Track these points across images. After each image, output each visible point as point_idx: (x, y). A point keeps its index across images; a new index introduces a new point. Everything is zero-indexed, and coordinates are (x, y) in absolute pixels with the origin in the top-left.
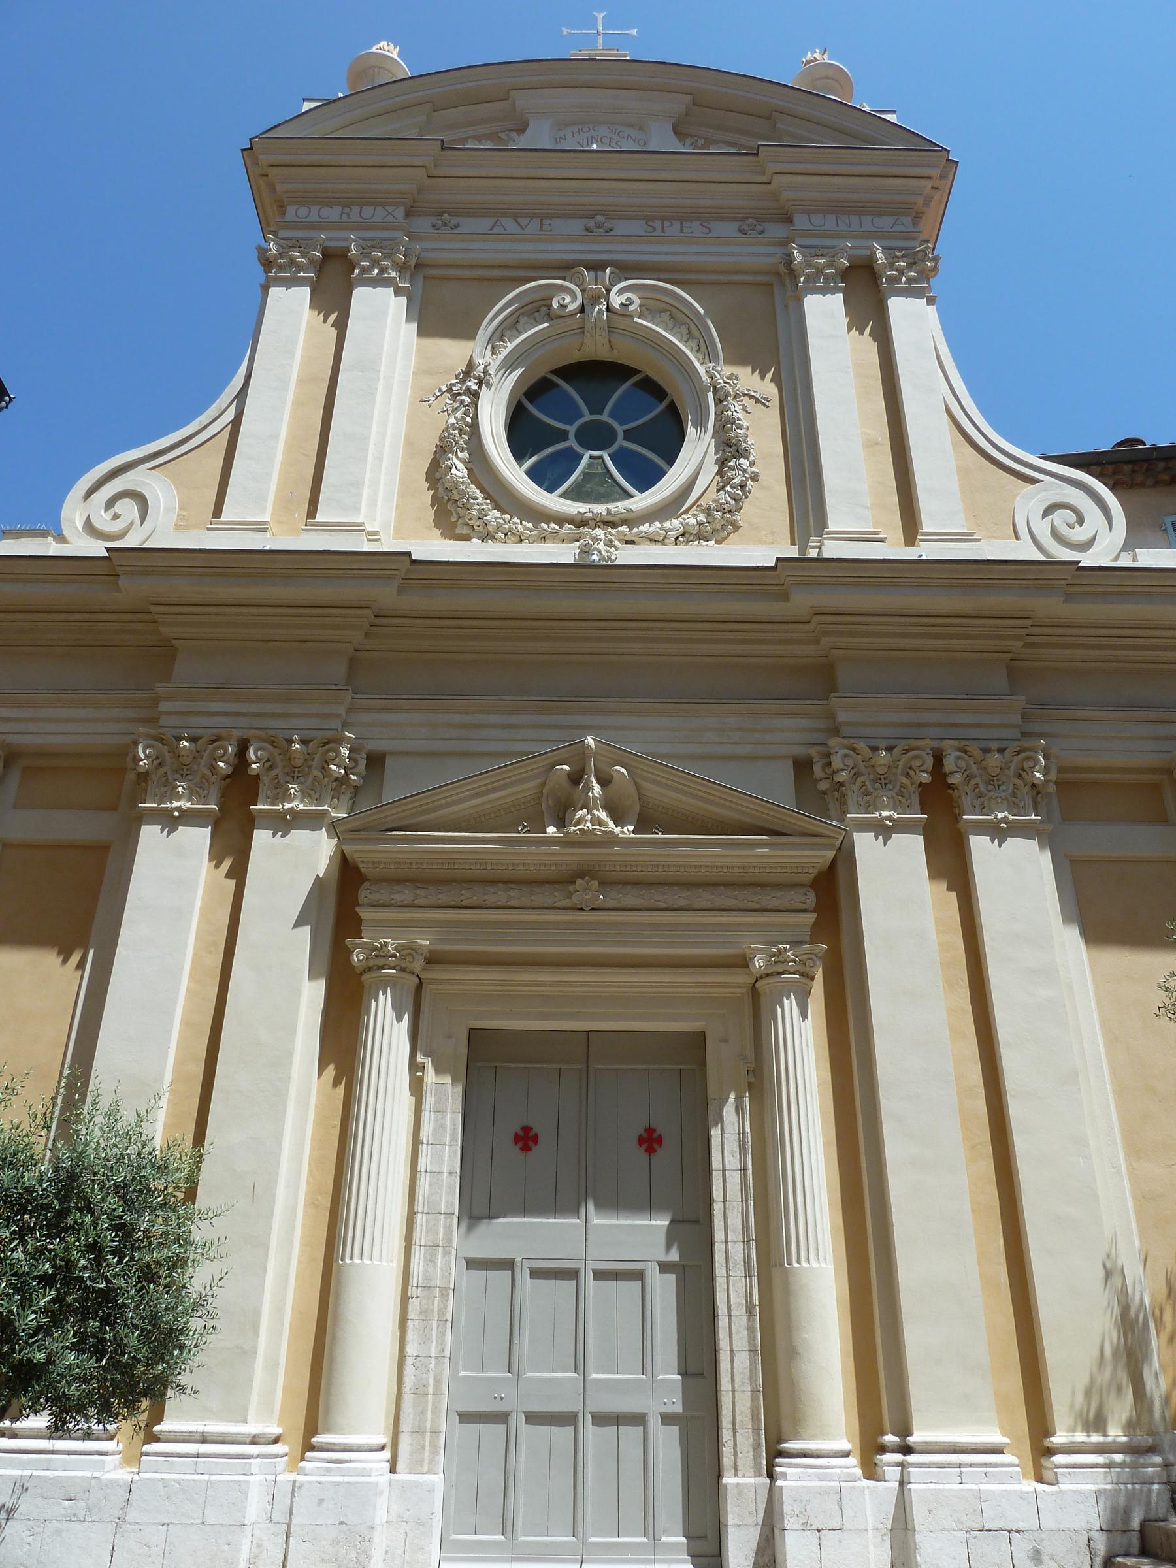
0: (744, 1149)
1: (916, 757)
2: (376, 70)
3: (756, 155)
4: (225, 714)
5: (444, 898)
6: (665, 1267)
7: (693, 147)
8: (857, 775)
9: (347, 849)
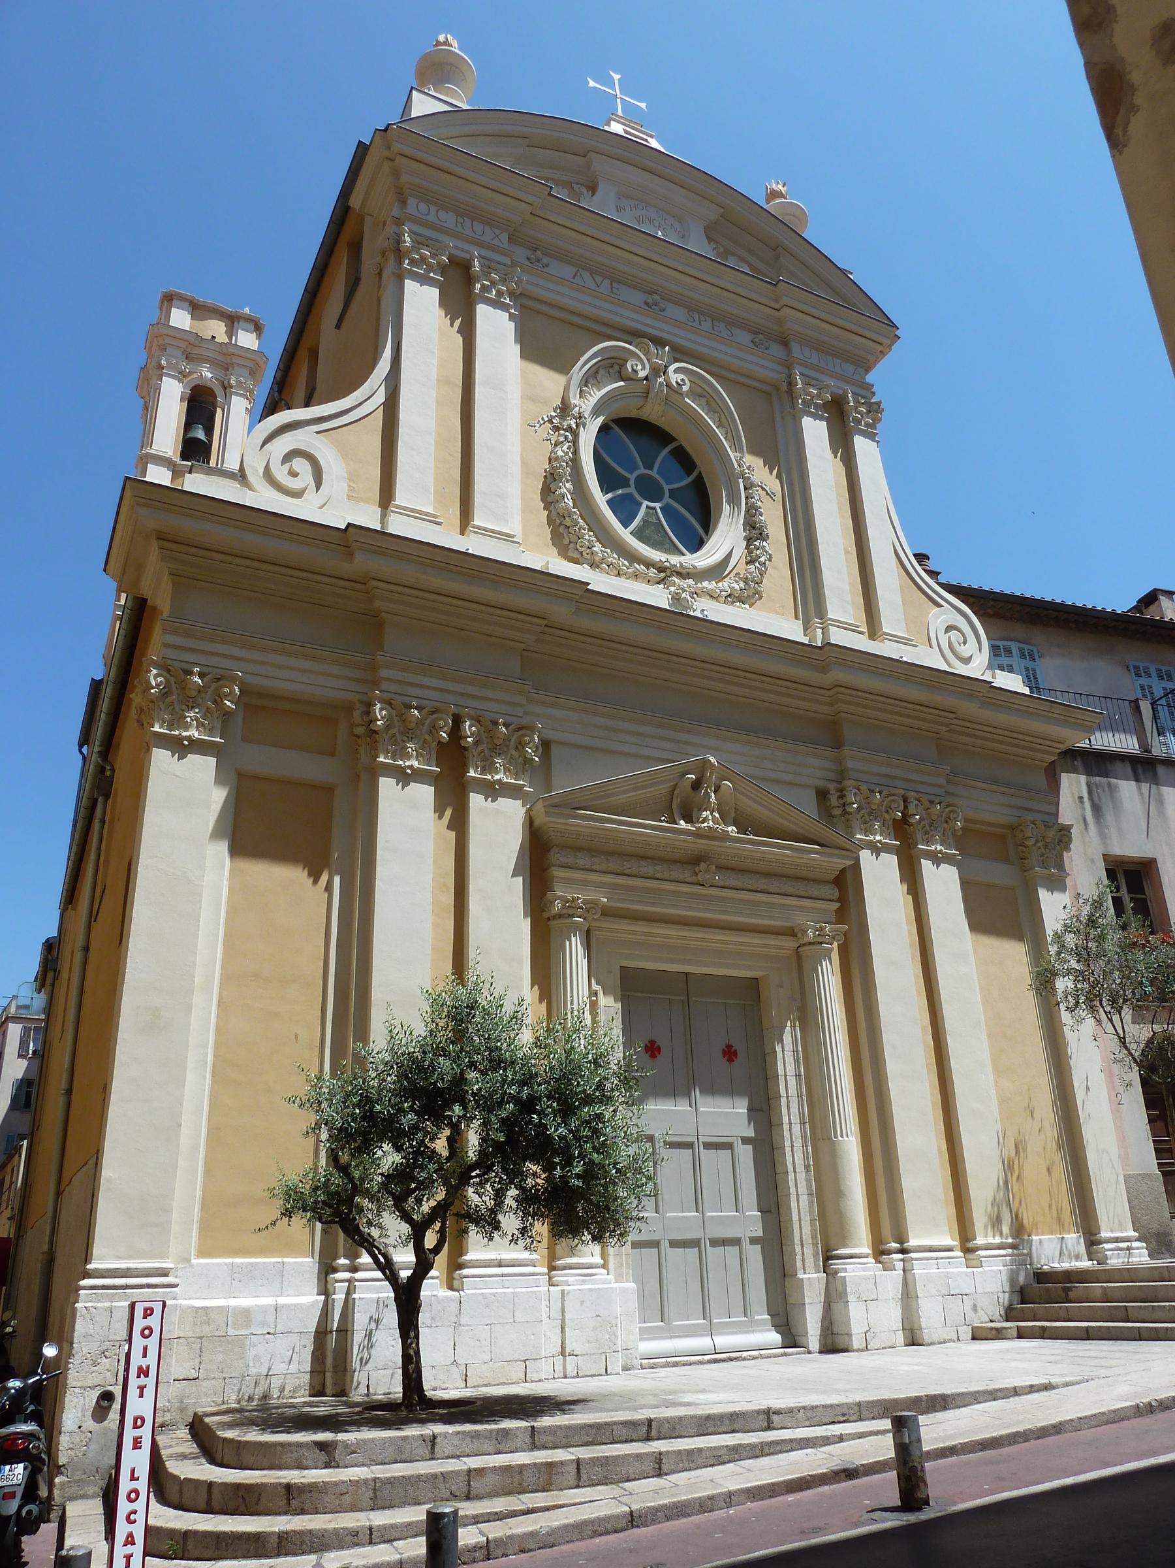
0: (798, 1062)
1: (893, 800)
2: (453, 68)
3: (775, 285)
4: (435, 689)
5: (612, 866)
6: (745, 1141)
9: (541, 819)
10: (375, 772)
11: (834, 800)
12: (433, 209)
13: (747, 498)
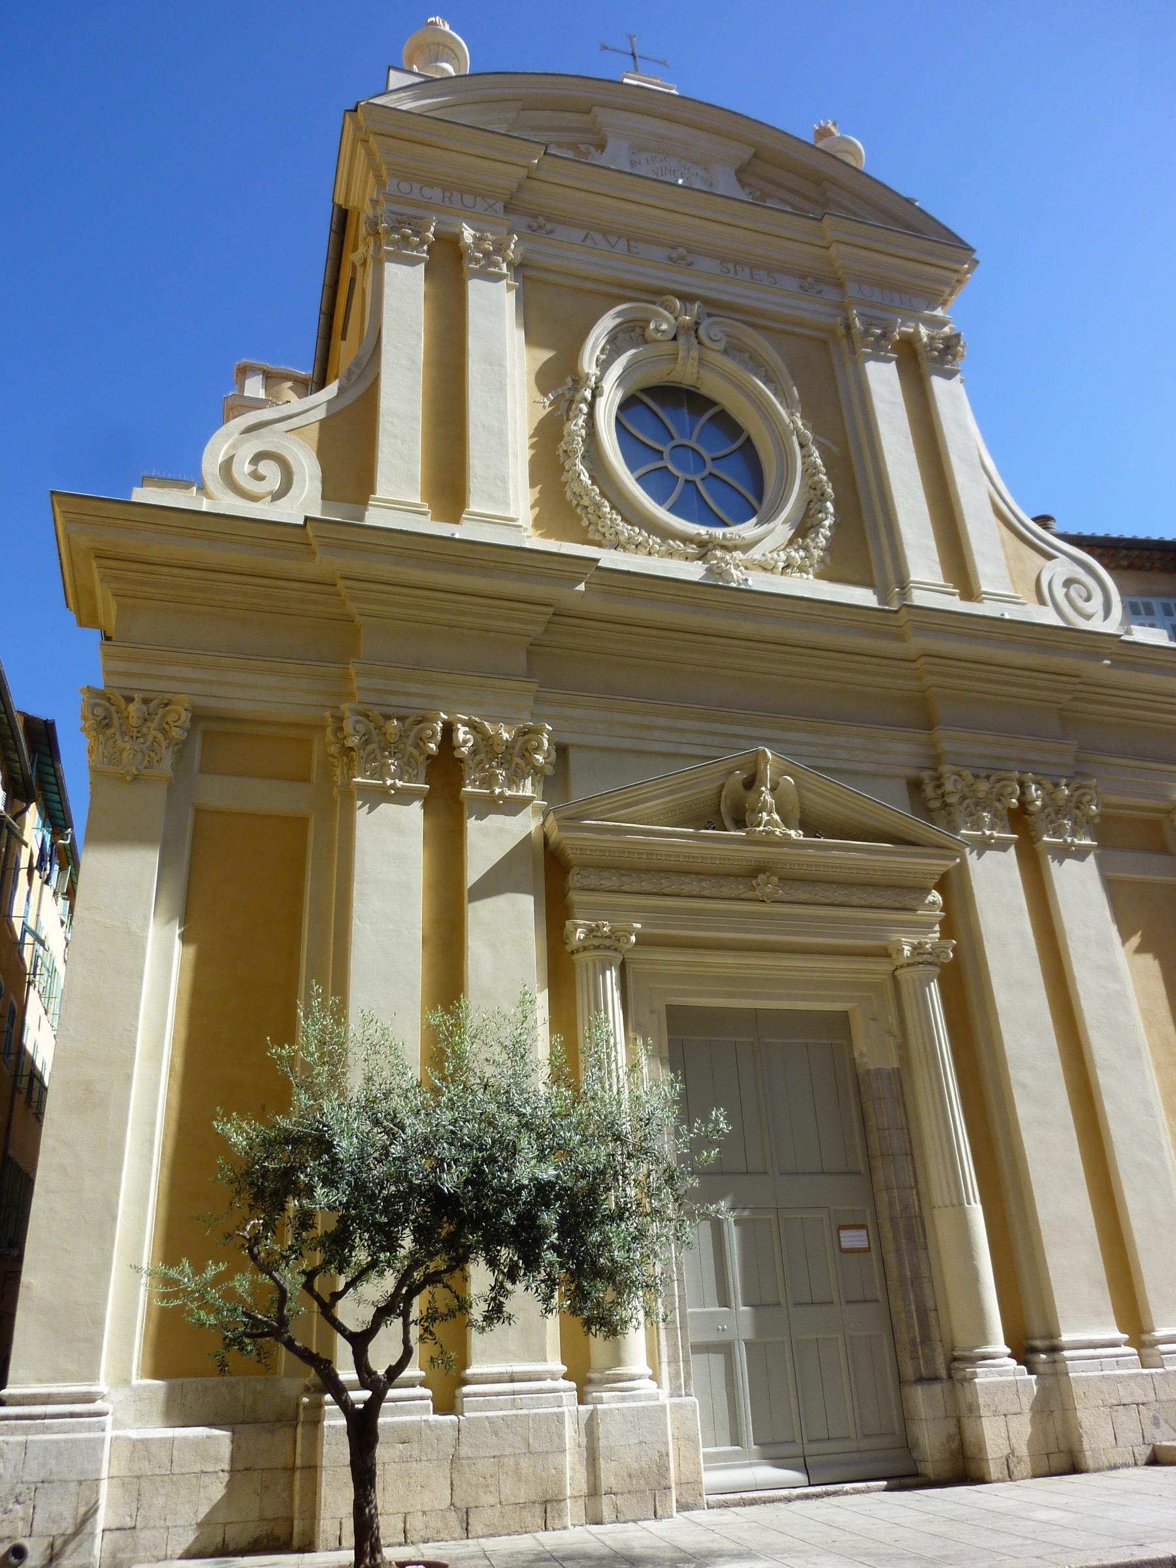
3: (820, 220)
7: (751, 196)
8: (367, 742)
10: (349, 796)
11: (929, 791)
12: (416, 187)
13: (804, 457)
